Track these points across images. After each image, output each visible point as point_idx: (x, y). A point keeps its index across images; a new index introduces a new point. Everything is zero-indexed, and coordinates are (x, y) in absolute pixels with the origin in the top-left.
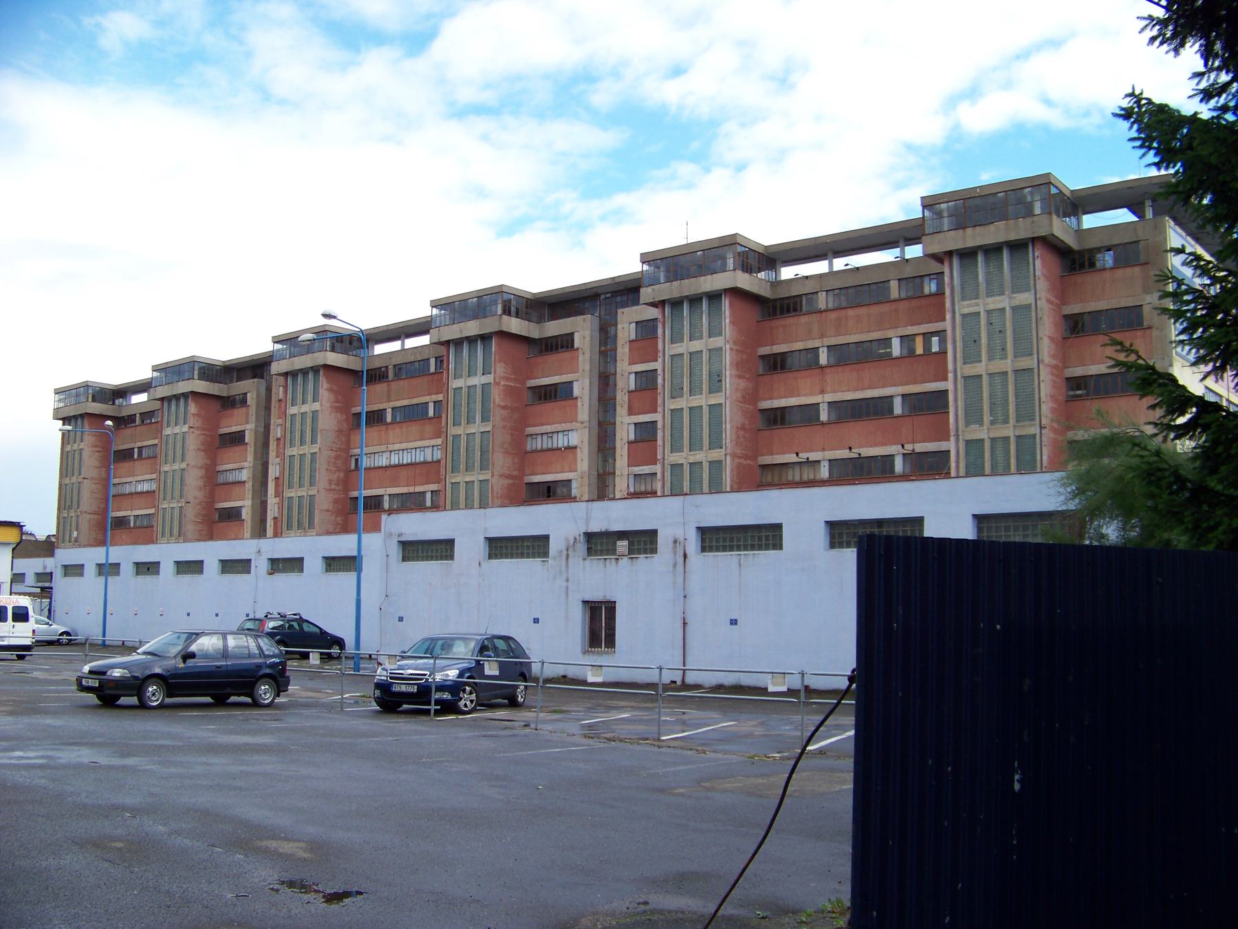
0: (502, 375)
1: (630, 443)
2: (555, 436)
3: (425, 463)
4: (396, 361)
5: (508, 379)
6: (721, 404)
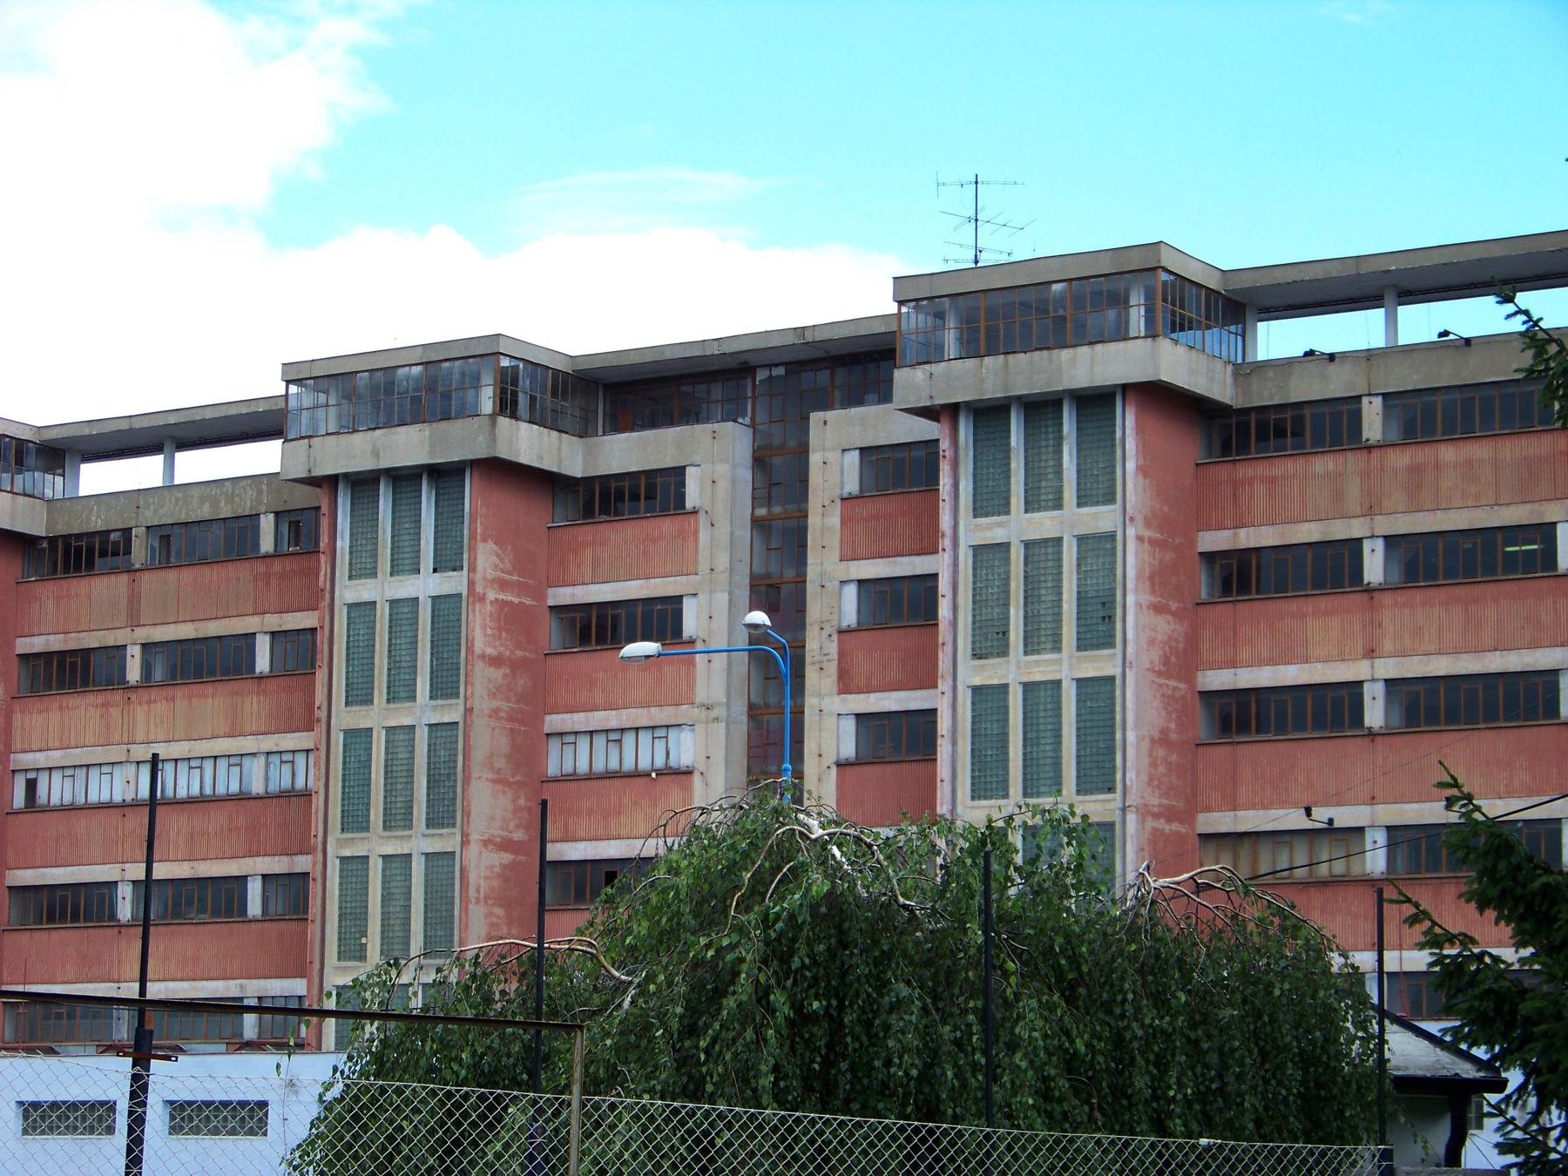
0: (491, 574)
1: (840, 765)
2: (629, 739)
3: (243, 797)
4: (151, 517)
5: (503, 585)
6: (1112, 678)
